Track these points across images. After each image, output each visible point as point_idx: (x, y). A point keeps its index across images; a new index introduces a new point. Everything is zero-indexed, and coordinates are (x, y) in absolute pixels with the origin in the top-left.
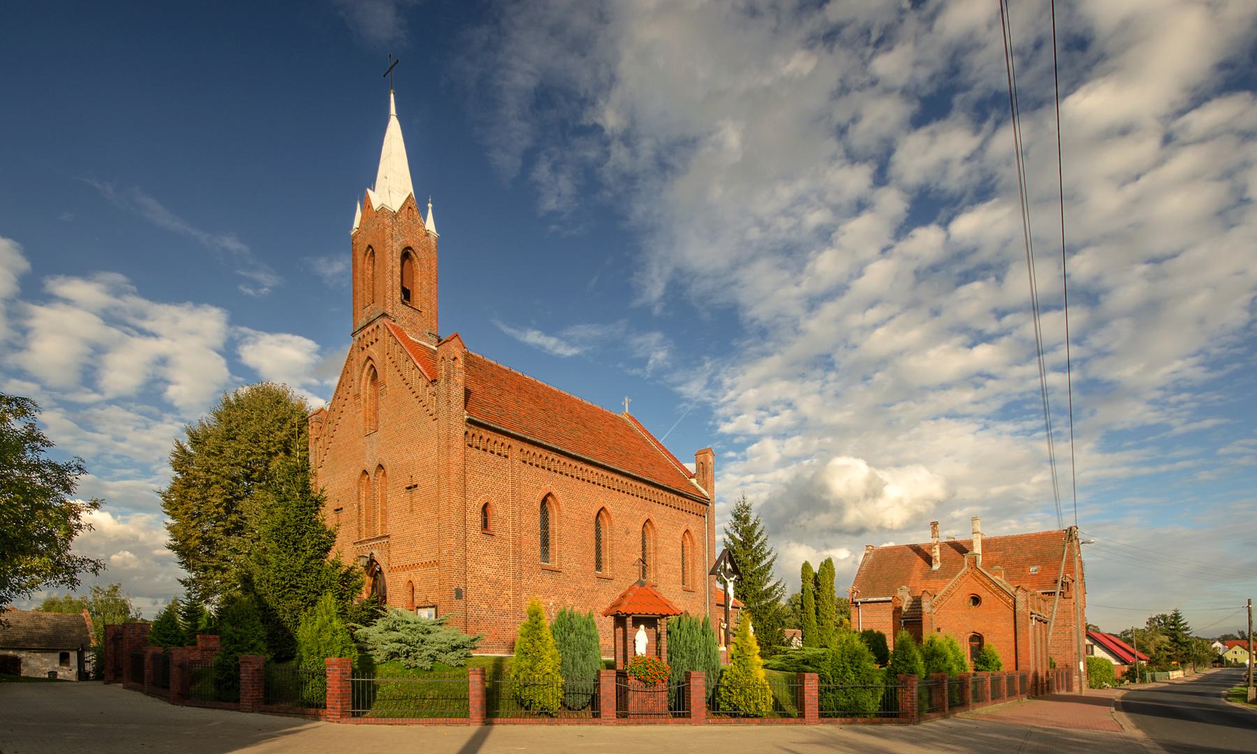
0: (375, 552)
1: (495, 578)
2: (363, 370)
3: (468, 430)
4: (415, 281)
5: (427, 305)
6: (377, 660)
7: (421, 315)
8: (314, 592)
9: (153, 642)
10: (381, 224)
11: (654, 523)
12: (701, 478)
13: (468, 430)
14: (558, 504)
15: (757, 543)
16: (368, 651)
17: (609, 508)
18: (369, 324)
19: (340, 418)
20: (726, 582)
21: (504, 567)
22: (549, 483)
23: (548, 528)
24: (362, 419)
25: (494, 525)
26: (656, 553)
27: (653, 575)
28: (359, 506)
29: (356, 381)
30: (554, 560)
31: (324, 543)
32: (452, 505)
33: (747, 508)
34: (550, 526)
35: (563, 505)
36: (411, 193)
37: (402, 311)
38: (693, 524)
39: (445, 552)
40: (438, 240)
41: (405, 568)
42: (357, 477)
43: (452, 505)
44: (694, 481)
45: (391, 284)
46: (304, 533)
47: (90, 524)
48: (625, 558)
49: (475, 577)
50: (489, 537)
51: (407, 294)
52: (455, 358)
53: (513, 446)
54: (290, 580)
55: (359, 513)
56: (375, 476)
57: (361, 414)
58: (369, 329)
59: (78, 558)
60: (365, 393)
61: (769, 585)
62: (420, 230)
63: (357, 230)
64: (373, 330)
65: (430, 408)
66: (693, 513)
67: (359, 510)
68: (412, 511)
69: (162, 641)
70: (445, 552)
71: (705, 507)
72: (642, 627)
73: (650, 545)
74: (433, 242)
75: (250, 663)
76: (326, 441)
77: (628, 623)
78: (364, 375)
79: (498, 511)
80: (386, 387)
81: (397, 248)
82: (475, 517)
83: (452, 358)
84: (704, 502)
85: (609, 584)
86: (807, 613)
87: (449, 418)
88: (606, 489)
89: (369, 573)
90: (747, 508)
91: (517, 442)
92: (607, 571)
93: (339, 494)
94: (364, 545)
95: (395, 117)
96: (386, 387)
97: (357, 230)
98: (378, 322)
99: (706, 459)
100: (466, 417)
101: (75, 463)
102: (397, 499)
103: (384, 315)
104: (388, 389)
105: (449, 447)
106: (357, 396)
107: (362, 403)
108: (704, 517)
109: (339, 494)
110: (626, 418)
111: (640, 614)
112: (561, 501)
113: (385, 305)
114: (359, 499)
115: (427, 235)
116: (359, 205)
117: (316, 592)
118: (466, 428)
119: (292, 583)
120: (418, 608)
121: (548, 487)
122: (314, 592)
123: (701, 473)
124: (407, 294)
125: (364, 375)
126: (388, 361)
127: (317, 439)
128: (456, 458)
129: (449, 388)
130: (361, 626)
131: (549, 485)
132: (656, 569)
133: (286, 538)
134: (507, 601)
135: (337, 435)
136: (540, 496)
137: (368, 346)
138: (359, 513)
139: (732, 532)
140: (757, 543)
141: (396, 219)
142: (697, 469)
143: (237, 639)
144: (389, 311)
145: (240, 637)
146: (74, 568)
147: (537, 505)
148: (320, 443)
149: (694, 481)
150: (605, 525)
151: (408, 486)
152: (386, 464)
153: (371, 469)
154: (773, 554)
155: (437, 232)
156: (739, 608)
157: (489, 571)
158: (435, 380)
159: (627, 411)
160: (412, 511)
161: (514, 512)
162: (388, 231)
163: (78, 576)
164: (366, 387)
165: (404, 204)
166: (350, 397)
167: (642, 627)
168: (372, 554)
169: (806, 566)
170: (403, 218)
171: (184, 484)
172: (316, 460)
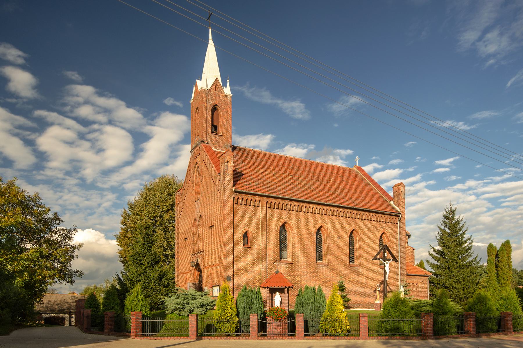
0: (199, 259)
1: (251, 269)
2: (195, 169)
3: (235, 196)
4: (220, 121)
5: (225, 132)
6: (167, 312)
7: (222, 138)
8: (146, 283)
9: (86, 307)
10: (201, 97)
11: (358, 231)
12: (396, 201)
13: (235, 196)
14: (291, 227)
15: (461, 232)
16: (165, 308)
17: (325, 225)
18: (196, 146)
19: (187, 193)
20: (384, 264)
21: (256, 264)
22: (281, 217)
23: (286, 240)
24: (194, 193)
25: (251, 242)
26: (360, 248)
27: (358, 261)
28: (193, 236)
29: (192, 175)
30: (289, 257)
31: (154, 260)
32: (225, 235)
33: (454, 212)
34: (288, 239)
35: (294, 228)
36: (216, 80)
37: (212, 137)
38: (389, 229)
39: (222, 258)
40: (232, 97)
41: (209, 267)
42: (192, 222)
43: (225, 235)
44: (392, 203)
45: (206, 125)
46: (145, 257)
47: (77, 255)
48: (337, 253)
49: (239, 270)
50: (248, 249)
51: (215, 128)
52: (228, 162)
53: (262, 201)
54: (136, 278)
55: (193, 240)
56: (199, 221)
57: (194, 191)
58: (196, 149)
59: (73, 270)
60: (196, 180)
61: (470, 259)
62: (222, 94)
63: (192, 100)
64: (198, 149)
65: (218, 187)
66: (388, 222)
67: (193, 238)
68: (212, 238)
69: (89, 307)
70: (222, 258)
71: (397, 218)
72: (277, 293)
73: (356, 244)
74: (229, 99)
75: (108, 315)
76: (182, 205)
77: (285, 291)
78: (195, 171)
79: (253, 235)
80: (203, 177)
81: (210, 107)
82: (239, 239)
83: (226, 161)
84: (397, 215)
85: (325, 268)
86: (489, 277)
87: (224, 192)
88: (324, 215)
89: (197, 270)
90: (454, 212)
91: (264, 198)
92: (325, 261)
93: (186, 231)
94: (195, 256)
95: (211, 40)
96: (203, 177)
97: (192, 100)
98: (200, 145)
99: (399, 189)
100: (234, 190)
101: (73, 228)
102: (206, 233)
103: (202, 142)
104: (203, 178)
105: (224, 206)
106: (192, 182)
107: (194, 185)
108: (397, 223)
109: (186, 231)
110: (356, 169)
111: (275, 287)
112: (293, 225)
113: (202, 137)
114: (193, 233)
115: (226, 96)
116: (194, 87)
117: (148, 283)
118: (234, 196)
119: (137, 279)
120: (213, 286)
121: (285, 219)
122: (146, 283)
123: (396, 196)
124: (215, 128)
125: (195, 171)
126: (203, 164)
127: (178, 204)
128: (229, 211)
129: (224, 177)
130: (164, 297)
131: (285, 218)
132: (360, 257)
133: (137, 259)
134: (258, 281)
135: (186, 201)
136: (279, 224)
137: (197, 157)
138: (193, 240)
139: (442, 227)
140: (461, 232)
141: (209, 92)
142: (394, 195)
143: (106, 305)
144: (205, 139)
145: (107, 304)
146: (72, 275)
147: (277, 229)
148: (179, 206)
149: (392, 203)
150: (324, 235)
151: (210, 226)
152: (203, 215)
153: (197, 217)
154: (472, 239)
155: (231, 94)
156: (428, 276)
157: (247, 266)
158: (219, 173)
159: (357, 165)
160: (212, 238)
161: (262, 235)
162: (204, 100)
163: (74, 279)
164: (196, 177)
165: (213, 84)
166: (190, 182)
167: (277, 293)
168: (197, 260)
169: (490, 246)
170: (213, 91)
171: (125, 231)
172: (178, 214)
